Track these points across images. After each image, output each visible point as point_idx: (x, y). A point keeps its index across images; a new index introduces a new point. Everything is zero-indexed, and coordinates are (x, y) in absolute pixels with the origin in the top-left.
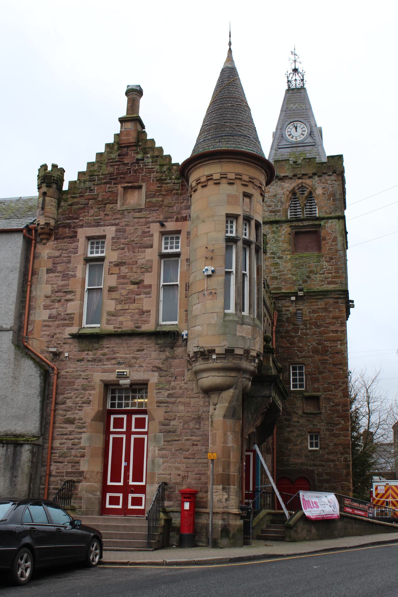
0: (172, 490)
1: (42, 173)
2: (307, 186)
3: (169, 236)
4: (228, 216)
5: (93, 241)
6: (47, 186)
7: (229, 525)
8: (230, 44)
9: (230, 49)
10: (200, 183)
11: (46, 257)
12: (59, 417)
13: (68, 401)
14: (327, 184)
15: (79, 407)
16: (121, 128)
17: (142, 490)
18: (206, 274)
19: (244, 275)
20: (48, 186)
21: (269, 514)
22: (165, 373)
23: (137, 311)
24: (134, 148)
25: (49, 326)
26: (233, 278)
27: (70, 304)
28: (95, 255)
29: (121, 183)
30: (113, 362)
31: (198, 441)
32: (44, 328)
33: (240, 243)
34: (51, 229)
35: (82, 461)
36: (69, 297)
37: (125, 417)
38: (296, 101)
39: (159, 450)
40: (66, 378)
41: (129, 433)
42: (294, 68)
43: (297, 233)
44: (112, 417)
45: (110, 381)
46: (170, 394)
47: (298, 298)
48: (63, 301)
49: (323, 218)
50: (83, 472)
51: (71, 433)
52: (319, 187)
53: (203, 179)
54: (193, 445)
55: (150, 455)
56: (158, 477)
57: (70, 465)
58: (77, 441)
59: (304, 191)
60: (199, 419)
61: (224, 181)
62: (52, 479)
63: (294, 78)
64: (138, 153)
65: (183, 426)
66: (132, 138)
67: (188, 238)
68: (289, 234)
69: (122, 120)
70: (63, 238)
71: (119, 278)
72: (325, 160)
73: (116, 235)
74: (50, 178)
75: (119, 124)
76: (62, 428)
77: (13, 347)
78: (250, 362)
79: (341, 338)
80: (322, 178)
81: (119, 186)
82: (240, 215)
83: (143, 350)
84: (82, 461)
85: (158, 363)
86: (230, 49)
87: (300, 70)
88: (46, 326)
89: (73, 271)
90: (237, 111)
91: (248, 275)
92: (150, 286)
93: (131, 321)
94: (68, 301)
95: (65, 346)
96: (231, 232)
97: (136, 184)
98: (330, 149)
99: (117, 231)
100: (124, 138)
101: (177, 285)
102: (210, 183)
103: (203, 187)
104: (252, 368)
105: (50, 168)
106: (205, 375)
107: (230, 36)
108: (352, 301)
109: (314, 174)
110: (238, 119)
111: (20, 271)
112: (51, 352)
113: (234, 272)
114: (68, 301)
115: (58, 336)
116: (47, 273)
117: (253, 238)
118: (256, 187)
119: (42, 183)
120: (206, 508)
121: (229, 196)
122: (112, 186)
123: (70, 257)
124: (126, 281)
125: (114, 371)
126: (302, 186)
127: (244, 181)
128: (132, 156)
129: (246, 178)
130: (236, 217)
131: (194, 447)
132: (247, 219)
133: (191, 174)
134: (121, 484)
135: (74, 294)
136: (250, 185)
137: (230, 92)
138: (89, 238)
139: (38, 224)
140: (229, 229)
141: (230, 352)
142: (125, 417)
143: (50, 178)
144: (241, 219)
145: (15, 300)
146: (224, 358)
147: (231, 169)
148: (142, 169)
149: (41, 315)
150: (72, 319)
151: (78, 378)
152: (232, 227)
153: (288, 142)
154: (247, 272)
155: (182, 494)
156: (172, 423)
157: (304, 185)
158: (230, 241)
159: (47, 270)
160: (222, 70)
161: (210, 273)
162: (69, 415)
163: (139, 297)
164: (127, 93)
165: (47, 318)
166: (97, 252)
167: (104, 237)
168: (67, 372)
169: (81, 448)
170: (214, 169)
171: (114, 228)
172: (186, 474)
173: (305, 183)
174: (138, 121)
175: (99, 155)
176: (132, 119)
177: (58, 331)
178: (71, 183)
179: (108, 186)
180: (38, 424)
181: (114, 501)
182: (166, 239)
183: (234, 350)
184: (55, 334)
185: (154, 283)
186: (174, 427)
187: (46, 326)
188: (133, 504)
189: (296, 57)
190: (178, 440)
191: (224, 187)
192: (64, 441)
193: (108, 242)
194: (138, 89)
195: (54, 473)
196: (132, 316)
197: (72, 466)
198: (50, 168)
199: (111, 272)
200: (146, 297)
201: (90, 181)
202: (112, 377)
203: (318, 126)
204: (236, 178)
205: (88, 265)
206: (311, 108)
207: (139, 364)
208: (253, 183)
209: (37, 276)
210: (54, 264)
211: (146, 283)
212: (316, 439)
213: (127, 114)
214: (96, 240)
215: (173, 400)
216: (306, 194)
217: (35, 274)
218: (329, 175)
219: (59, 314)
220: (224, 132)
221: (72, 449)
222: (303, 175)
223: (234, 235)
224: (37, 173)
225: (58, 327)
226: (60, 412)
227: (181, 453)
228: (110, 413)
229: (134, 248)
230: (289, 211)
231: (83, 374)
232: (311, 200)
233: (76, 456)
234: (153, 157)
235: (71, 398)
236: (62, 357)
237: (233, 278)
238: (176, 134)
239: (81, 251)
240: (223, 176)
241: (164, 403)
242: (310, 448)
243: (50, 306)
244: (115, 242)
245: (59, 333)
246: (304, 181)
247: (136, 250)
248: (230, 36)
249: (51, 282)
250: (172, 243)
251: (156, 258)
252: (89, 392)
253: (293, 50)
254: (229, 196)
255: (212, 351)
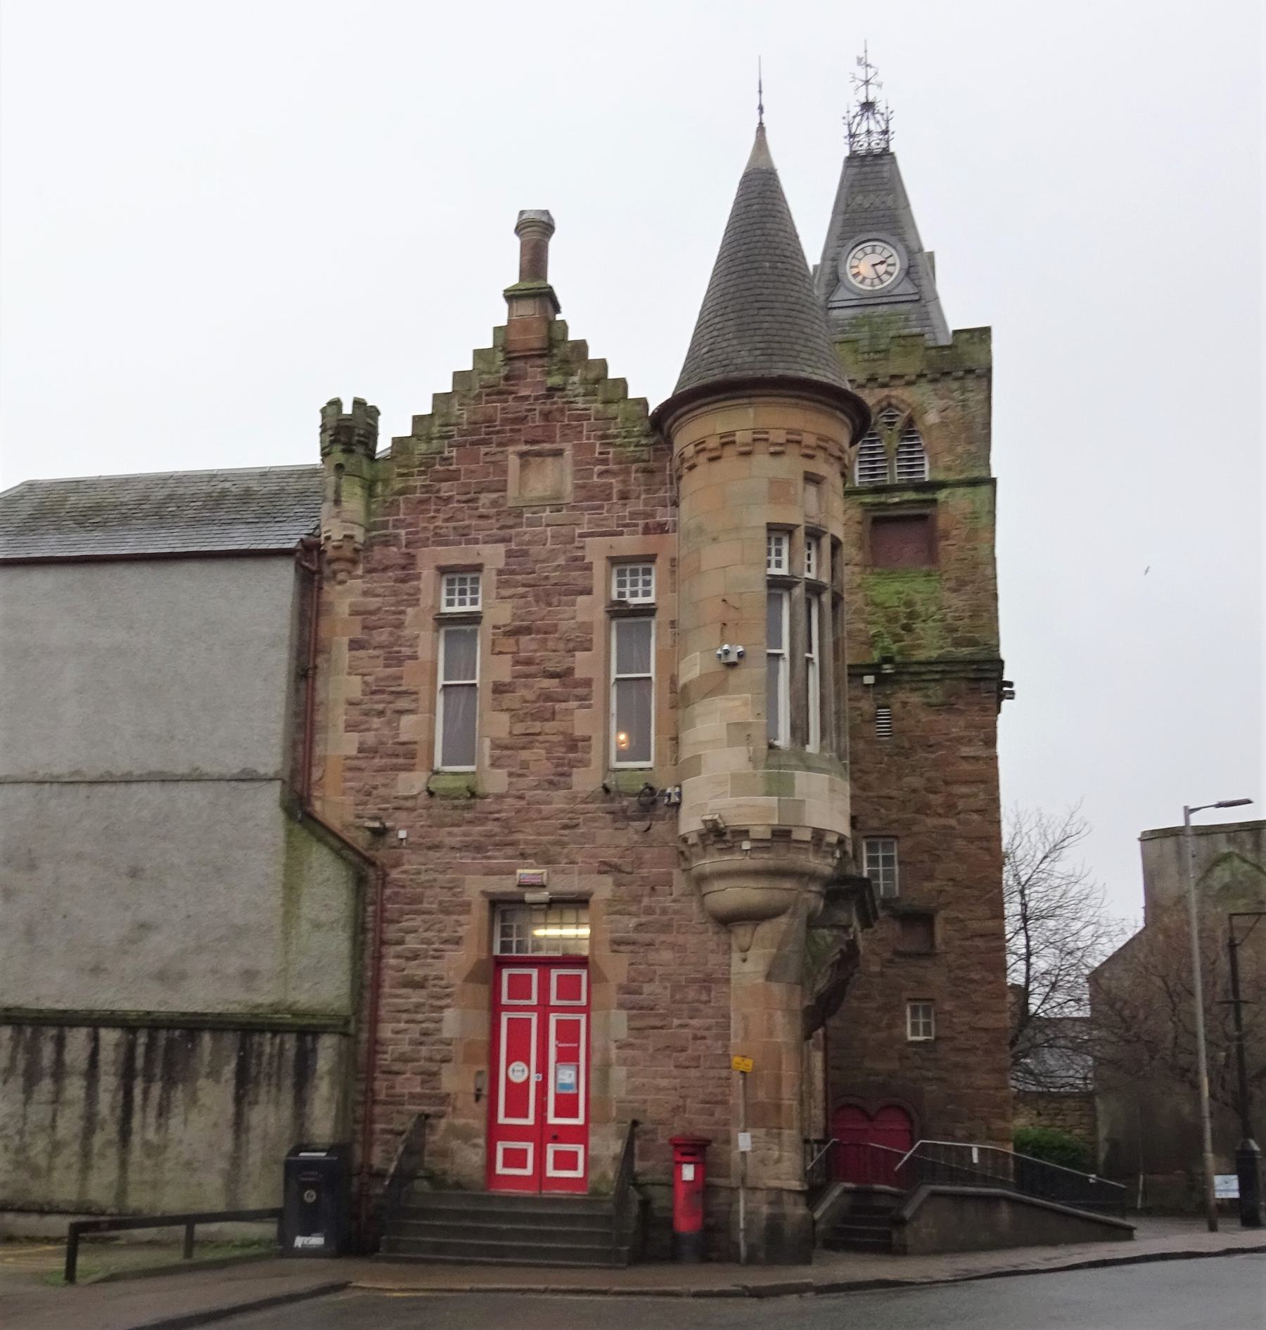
0: (647, 1137)
1: (332, 423)
2: (902, 406)
3: (629, 567)
4: (772, 528)
5: (450, 576)
6: (344, 451)
7: (783, 1216)
8: (761, 108)
9: (761, 124)
10: (703, 450)
11: (347, 610)
12: (391, 972)
13: (409, 938)
14: (953, 399)
15: (436, 950)
16: (510, 314)
17: (579, 1135)
18: (724, 660)
19: (809, 660)
20: (348, 450)
21: (847, 1191)
22: (629, 877)
23: (560, 738)
24: (539, 362)
25: (359, 769)
26: (784, 668)
27: (406, 720)
28: (457, 609)
29: (512, 442)
30: (510, 851)
31: (708, 1029)
32: (349, 775)
33: (799, 591)
34: (356, 551)
35: (446, 1070)
36: (402, 704)
37: (534, 973)
38: (872, 191)
39: (619, 1048)
40: (403, 887)
41: (544, 1009)
42: (864, 100)
43: (877, 521)
44: (506, 973)
45: (504, 894)
46: (641, 925)
47: (882, 679)
48: (389, 713)
49: (940, 485)
50: (448, 1095)
51: (418, 1007)
52: (932, 407)
53: (713, 443)
54: (695, 1038)
55: (596, 1060)
56: (618, 1108)
57: (419, 1078)
58: (431, 1026)
59: (893, 417)
60: (708, 982)
61: (761, 446)
62: (378, 1109)
63: (863, 128)
64: (549, 373)
65: (672, 996)
66: (535, 340)
67: (673, 572)
68: (859, 523)
69: (512, 296)
70: (385, 569)
71: (517, 663)
72: (945, 341)
73: (507, 564)
74: (348, 430)
75: (505, 306)
76: (393, 998)
77: (280, 816)
78: (824, 857)
79: (986, 777)
80: (939, 386)
81: (511, 449)
82: (798, 526)
83: (577, 825)
84: (446, 1070)
85: (611, 855)
86: (761, 124)
87: (880, 107)
88: (350, 769)
89: (411, 646)
90: (784, 279)
91: (816, 660)
92: (588, 683)
93: (548, 759)
94: (400, 712)
95: (398, 814)
96: (779, 564)
97: (547, 446)
98: (958, 314)
99: (509, 554)
100: (514, 336)
101: (650, 678)
102: (729, 451)
103: (712, 459)
104: (828, 871)
105: (347, 409)
106: (717, 885)
107: (760, 92)
108: (1010, 684)
109: (921, 376)
110: (790, 299)
111: (291, 646)
112: (370, 829)
113: (787, 656)
114: (400, 712)
115: (382, 791)
116: (351, 649)
117: (825, 579)
118: (832, 460)
119: (332, 442)
120: (728, 1176)
121: (773, 482)
122: (494, 449)
123: (403, 612)
124: (532, 669)
125: (513, 873)
126: (890, 405)
127: (807, 447)
128: (535, 378)
129: (810, 440)
130: (789, 530)
131: (698, 1042)
132: (814, 535)
133: (680, 427)
134: (530, 1121)
135: (414, 697)
136: (820, 455)
137: (766, 232)
138: (443, 570)
139: (328, 538)
140: (773, 558)
141: (781, 835)
142: (534, 973)
143: (348, 430)
144: (800, 535)
145: (282, 711)
146: (767, 849)
147: (779, 418)
148: (562, 411)
149: (339, 743)
150: (412, 755)
151: (431, 887)
152: (779, 553)
153: (851, 291)
154: (815, 655)
155: (676, 1145)
156: (647, 988)
157: (894, 401)
158: (778, 585)
159: (351, 641)
160: (746, 176)
161: (733, 658)
162: (415, 970)
163: (564, 705)
164: (518, 230)
165: (354, 752)
166: (462, 603)
167: (478, 568)
168: (404, 872)
169: (442, 1042)
170: (739, 420)
171: (501, 548)
172: (681, 1102)
173: (896, 397)
174: (548, 299)
175: (459, 377)
176: (533, 293)
177: (380, 780)
178: (397, 441)
179: (484, 450)
180: (345, 989)
181: (515, 1158)
182: (621, 573)
183: (790, 832)
184: (375, 788)
185: (597, 676)
186: (652, 997)
187: (350, 769)
188: (557, 1166)
189: (871, 72)
190: (661, 1028)
191: (764, 466)
192: (402, 1026)
193: (488, 578)
194: (544, 219)
195: (382, 1096)
196: (549, 751)
197: (423, 1082)
198: (347, 409)
199: (497, 650)
200: (581, 707)
201: (441, 438)
202: (505, 885)
203: (927, 249)
204: (788, 441)
205: (442, 632)
206: (908, 206)
207: (567, 857)
208: (825, 449)
209: (326, 656)
210: (365, 627)
211: (579, 674)
212: (927, 1015)
213: (522, 279)
214: (460, 575)
215: (647, 937)
216: (898, 426)
217: (322, 652)
218: (956, 379)
219: (382, 743)
220: (758, 332)
221: (421, 1044)
222: (893, 377)
223: (783, 571)
224: (318, 420)
225: (381, 770)
226: (393, 961)
227: (669, 1057)
228: (500, 963)
229: (548, 595)
230: (857, 467)
231: (440, 877)
232: (912, 439)
233: (430, 1060)
234: (584, 381)
235: (415, 931)
236: (391, 840)
237: (784, 668)
238: (642, 334)
239: (426, 600)
240: (760, 438)
241: (628, 944)
242: (911, 1038)
243: (362, 723)
244: (507, 582)
245: (384, 785)
246: (894, 393)
247: (555, 600)
248: (760, 92)
249: (360, 671)
250: (634, 584)
251: (600, 615)
252: (455, 917)
253: (862, 55)
254: (773, 482)
255: (744, 833)
